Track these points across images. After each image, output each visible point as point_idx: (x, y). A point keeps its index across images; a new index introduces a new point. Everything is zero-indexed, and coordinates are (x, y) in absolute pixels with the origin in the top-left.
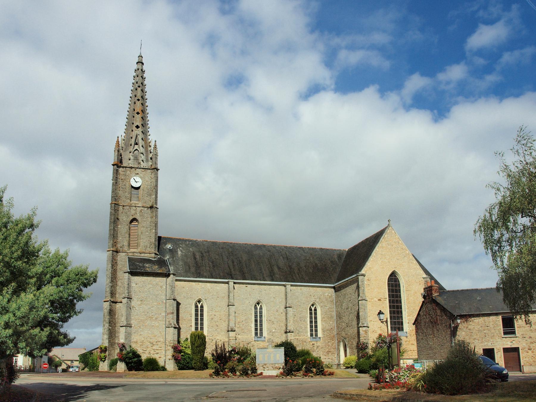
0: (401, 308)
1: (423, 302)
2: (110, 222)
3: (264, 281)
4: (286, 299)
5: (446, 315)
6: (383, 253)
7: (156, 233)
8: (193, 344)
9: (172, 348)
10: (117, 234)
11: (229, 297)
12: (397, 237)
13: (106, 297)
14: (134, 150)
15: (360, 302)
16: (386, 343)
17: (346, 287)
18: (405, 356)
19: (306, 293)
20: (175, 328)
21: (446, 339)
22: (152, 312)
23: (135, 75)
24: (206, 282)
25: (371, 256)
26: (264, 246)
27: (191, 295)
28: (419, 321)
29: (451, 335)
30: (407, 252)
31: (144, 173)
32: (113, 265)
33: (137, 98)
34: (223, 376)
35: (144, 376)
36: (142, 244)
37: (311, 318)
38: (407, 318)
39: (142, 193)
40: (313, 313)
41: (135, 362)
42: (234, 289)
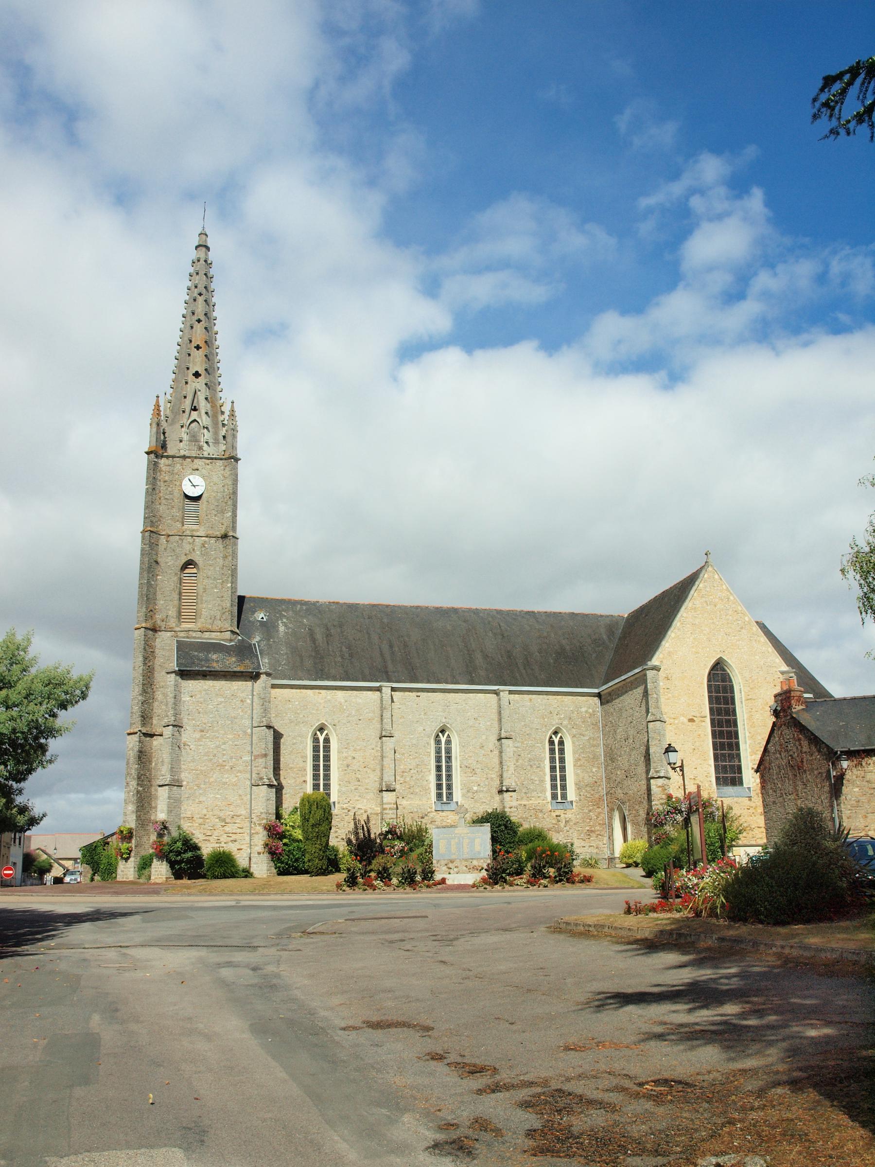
0: (737, 737)
1: (774, 724)
2: (141, 568)
3: (455, 684)
4: (500, 720)
5: (819, 751)
6: (697, 621)
7: (234, 589)
8: (305, 819)
9: (265, 828)
10: (155, 594)
11: (382, 720)
12: (724, 587)
13: (131, 724)
14: (190, 421)
15: (651, 725)
16: (681, 812)
17: (623, 694)
18: (743, 839)
19: (541, 708)
20: (270, 786)
21: (822, 801)
22: (224, 755)
23: (192, 271)
24: (336, 689)
25: (672, 629)
26: (455, 610)
27: (304, 716)
28: (767, 765)
29: (831, 794)
30: (746, 619)
31: (208, 467)
32: (145, 658)
33: (196, 318)
34: (363, 887)
35: (203, 889)
36: (205, 612)
37: (552, 760)
38: (749, 758)
39: (205, 509)
40: (557, 749)
41: (189, 861)
42: (393, 701)
